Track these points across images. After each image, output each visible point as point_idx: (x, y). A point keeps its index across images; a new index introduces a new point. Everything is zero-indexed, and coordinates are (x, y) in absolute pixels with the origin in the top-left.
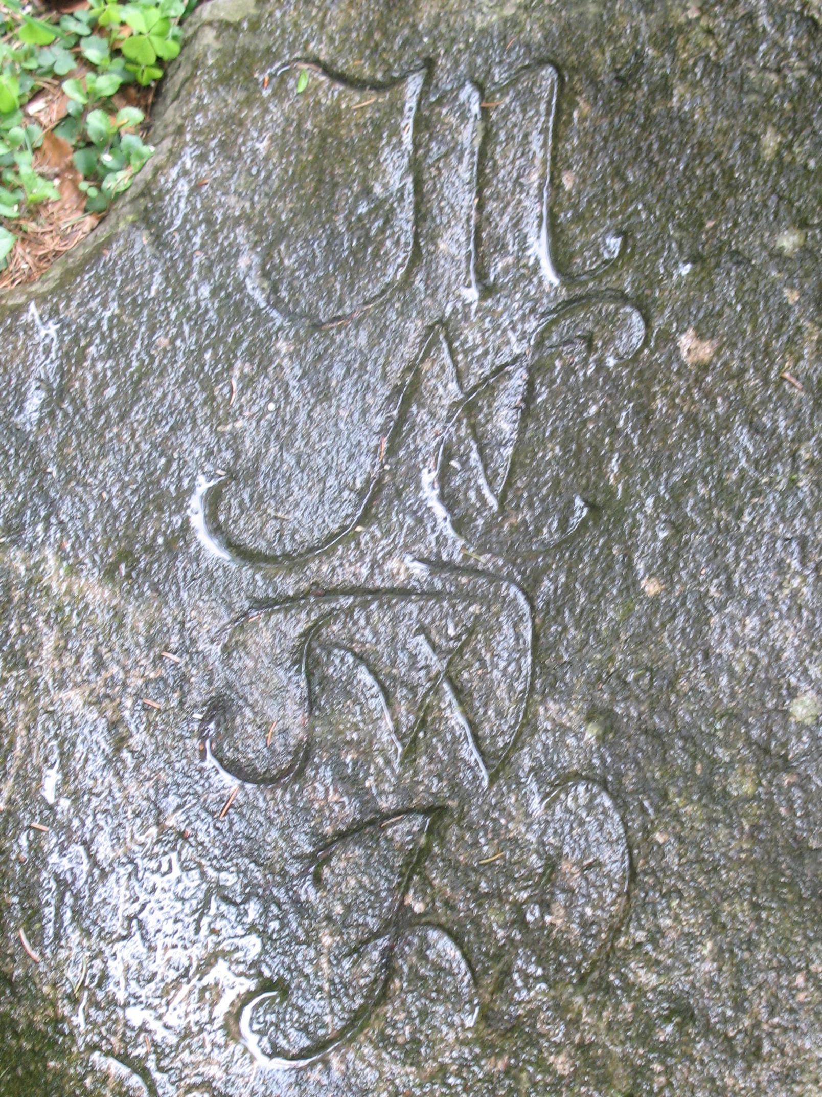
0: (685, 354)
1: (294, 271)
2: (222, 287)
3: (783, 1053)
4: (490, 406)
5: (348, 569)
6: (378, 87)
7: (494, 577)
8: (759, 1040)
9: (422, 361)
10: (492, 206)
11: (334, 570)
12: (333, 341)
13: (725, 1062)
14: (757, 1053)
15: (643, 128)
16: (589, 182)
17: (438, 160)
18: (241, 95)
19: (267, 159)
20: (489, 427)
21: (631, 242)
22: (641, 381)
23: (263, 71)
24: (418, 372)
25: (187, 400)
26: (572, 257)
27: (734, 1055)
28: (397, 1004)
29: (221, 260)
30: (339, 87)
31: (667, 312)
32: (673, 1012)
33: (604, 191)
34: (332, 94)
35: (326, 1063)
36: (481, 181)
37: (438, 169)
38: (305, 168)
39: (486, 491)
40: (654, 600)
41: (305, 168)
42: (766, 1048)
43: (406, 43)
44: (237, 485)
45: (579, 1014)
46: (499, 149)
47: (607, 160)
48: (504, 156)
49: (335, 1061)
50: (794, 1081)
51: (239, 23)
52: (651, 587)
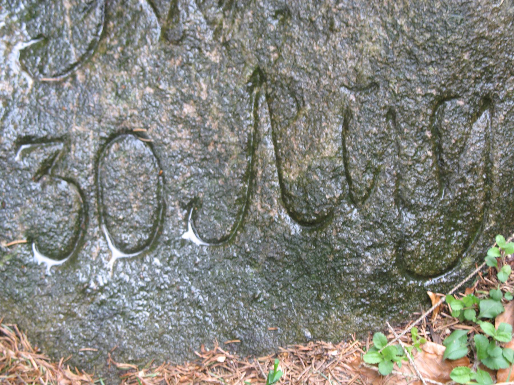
3: (347, 25)
8: (332, 19)
13: (313, 38)
14: (332, 29)
27: (317, 31)
28: (113, 35)
32: (278, 12)
35: (74, 76)
42: (337, 24)
45: (221, 24)
49: (80, 77)
50: (357, 41)
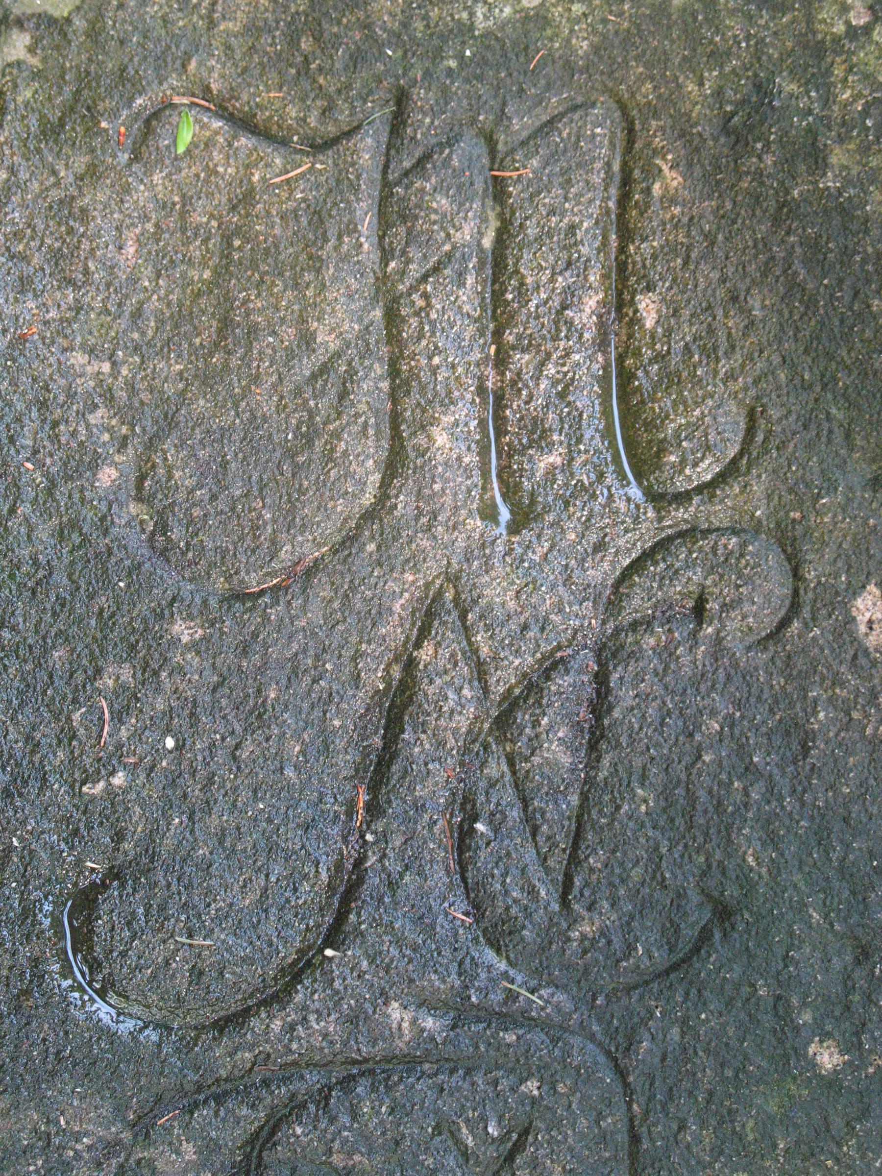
0: (863, 629)
1: (191, 491)
2: (74, 525)
4: (536, 724)
5: (312, 1026)
6: (319, 146)
7: (556, 1031)
9: (418, 645)
10: (521, 360)
11: (292, 1028)
12: (266, 618)
15: (776, 221)
16: (686, 313)
17: (425, 278)
18: (81, 162)
19: (133, 280)
20: (536, 760)
21: (762, 423)
22: (789, 678)
23: (114, 114)
24: (410, 665)
25: (28, 738)
26: (661, 452)
29: (68, 478)
30: (244, 142)
31: (829, 554)
33: (711, 330)
34: (236, 158)
36: (498, 313)
37: (426, 296)
38: (198, 295)
39: (535, 873)
40: (831, 1083)
41: (198, 295)
43: (356, 59)
44: (122, 886)
46: (527, 256)
47: (715, 275)
48: (534, 267)
51: (68, 20)
52: (828, 1058)
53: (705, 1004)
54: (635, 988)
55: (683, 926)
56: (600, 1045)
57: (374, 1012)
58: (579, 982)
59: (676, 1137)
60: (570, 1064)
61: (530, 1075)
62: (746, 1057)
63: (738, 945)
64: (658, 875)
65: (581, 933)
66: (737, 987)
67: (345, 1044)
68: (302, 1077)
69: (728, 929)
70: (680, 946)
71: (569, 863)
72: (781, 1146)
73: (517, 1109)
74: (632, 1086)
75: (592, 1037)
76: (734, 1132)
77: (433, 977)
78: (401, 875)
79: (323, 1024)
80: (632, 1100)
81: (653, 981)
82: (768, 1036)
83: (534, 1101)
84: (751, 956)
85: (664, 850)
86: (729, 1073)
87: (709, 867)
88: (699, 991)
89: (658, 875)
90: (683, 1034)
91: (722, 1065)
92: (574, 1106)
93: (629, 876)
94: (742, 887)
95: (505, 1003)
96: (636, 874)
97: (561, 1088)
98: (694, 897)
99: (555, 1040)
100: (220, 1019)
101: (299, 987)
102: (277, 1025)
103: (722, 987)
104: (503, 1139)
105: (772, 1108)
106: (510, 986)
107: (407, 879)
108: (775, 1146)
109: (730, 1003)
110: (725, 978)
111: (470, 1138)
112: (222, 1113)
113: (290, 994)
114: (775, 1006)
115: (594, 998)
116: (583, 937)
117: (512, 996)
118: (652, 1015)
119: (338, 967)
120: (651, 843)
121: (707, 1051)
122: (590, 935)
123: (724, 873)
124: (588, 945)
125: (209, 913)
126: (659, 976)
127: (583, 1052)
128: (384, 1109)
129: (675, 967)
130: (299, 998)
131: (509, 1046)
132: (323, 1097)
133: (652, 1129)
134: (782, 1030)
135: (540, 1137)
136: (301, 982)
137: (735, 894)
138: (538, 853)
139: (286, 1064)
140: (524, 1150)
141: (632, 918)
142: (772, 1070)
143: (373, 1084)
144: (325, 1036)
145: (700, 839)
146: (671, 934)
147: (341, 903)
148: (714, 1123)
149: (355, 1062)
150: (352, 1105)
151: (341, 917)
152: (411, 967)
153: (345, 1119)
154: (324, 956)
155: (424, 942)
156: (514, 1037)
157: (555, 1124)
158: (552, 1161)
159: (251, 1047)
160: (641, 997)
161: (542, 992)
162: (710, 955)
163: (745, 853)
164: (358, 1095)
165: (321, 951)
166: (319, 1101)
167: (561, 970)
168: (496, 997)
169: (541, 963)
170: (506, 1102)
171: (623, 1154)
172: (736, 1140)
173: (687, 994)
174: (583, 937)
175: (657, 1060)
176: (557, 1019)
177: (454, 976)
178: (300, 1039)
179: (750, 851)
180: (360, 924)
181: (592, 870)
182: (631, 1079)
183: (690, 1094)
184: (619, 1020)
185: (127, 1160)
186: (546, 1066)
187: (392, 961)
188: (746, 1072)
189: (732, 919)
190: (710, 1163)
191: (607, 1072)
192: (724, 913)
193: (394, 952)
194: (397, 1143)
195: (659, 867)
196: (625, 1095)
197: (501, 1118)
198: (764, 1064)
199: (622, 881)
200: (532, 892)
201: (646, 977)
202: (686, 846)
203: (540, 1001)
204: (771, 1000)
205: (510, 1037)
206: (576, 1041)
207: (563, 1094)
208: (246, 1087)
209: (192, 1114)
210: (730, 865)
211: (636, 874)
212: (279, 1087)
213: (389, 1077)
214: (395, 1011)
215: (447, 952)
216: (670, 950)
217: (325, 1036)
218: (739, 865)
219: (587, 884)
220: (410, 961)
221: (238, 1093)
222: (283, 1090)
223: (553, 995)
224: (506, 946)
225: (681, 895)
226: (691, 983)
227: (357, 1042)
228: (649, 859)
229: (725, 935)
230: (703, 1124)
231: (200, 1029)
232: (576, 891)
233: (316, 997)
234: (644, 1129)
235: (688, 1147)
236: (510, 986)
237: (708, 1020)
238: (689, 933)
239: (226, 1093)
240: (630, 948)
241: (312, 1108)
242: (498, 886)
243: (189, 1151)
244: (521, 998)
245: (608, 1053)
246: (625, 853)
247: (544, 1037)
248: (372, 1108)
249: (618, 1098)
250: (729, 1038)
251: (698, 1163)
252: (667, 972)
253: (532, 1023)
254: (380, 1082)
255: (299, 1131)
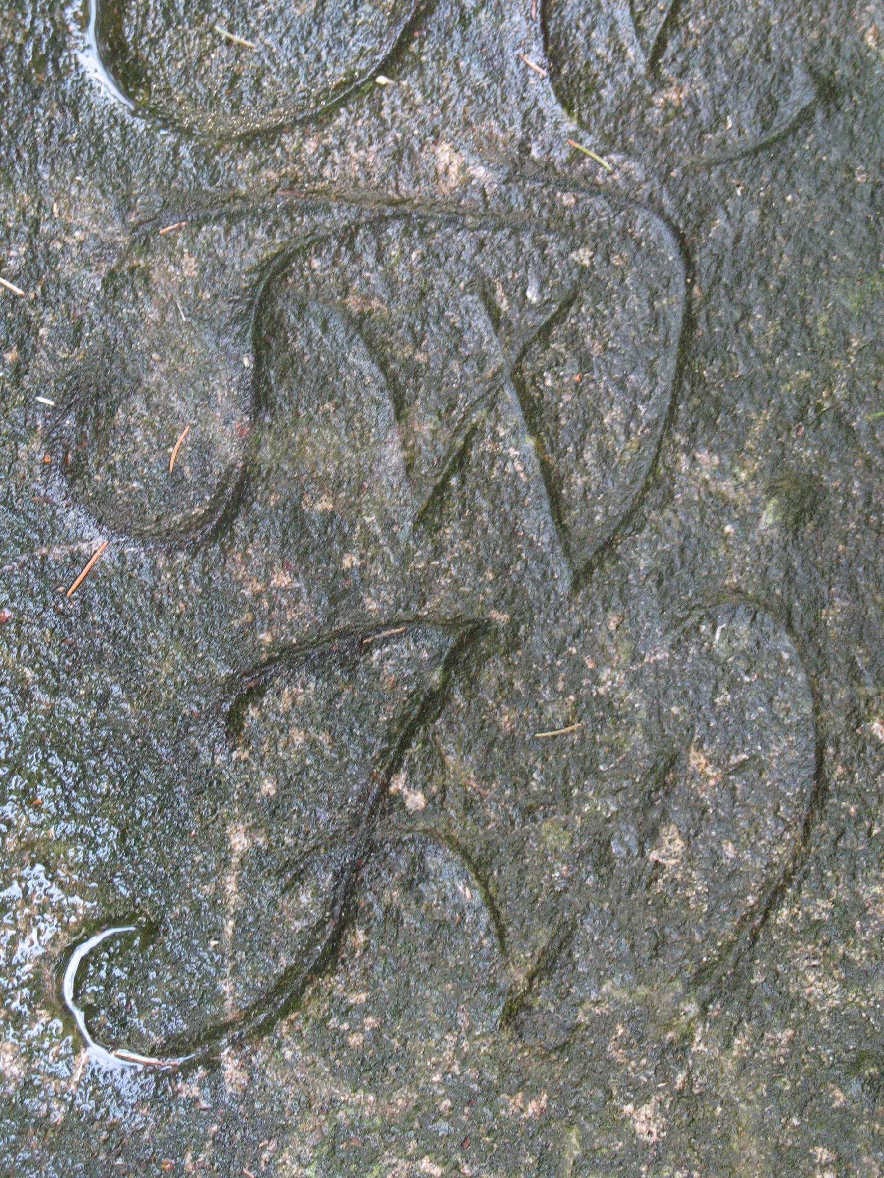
5: (352, 154)
7: (621, 200)
11: (327, 151)
39: (626, 31)
53: (793, 186)
54: (717, 164)
55: (782, 103)
56: (668, 220)
57: (421, 150)
58: (655, 152)
59: (736, 325)
60: (631, 234)
61: (584, 242)
62: (831, 245)
63: (840, 127)
64: (764, 47)
65: (666, 100)
66: (833, 170)
67: (383, 178)
68: (328, 210)
69: (833, 110)
70: (775, 124)
71: (665, 25)
72: (855, 344)
73: (563, 277)
74: (697, 267)
75: (660, 212)
76: (804, 325)
77: (493, 123)
78: (476, 12)
79: (362, 153)
80: (693, 282)
81: (739, 158)
82: (859, 226)
83: (583, 270)
84: (854, 140)
85: (774, 21)
86: (809, 261)
87: (822, 43)
88: (789, 172)
89: (764, 47)
90: (763, 215)
91: (802, 253)
92: (628, 281)
93: (730, 45)
94: (855, 67)
95: (569, 162)
96: (739, 43)
97: (615, 260)
98: (799, 74)
99: (617, 209)
100: (248, 133)
101: (342, 110)
102: (310, 146)
103: (817, 168)
104: (544, 305)
105: (851, 305)
106: (577, 146)
107: (482, 15)
108: (848, 344)
109: (821, 188)
110: (820, 160)
111: (505, 302)
112: (234, 232)
113: (331, 116)
114: (873, 194)
115: (670, 170)
116: (668, 105)
117: (577, 157)
118: (731, 194)
119: (389, 96)
120: (761, 13)
121: (787, 236)
122: (676, 104)
123: (838, 51)
124: (672, 112)
125: (256, 13)
126: (746, 154)
127: (649, 227)
128: (414, 256)
129: (765, 146)
130: (341, 121)
131: (565, 208)
132: (348, 236)
133: (712, 314)
134: (877, 221)
135: (583, 309)
136: (345, 106)
137: (847, 74)
138: (632, 12)
139: (314, 192)
140: (564, 321)
141: (726, 89)
142: (858, 263)
143: (406, 229)
144: (363, 165)
145: (817, 14)
146: (769, 107)
147: (403, 33)
148: (782, 313)
149: (392, 203)
150: (379, 245)
151: (401, 47)
152: (470, 109)
153: (369, 259)
154: (376, 84)
155: (489, 86)
156: (573, 200)
157: (602, 296)
158: (593, 337)
159: (277, 165)
160: (723, 174)
161: (612, 156)
162: (807, 135)
163: (865, 31)
164: (388, 236)
165: (373, 78)
166: (343, 238)
167: (637, 137)
168: (560, 156)
169: (616, 128)
170: (552, 268)
171: (674, 340)
172: (804, 335)
173: (774, 175)
174: (668, 105)
175: (728, 242)
176: (624, 187)
177: (517, 125)
178: (334, 163)
179: (871, 30)
180: (421, 54)
181: (688, 34)
182: (697, 258)
183: (762, 280)
184: (693, 196)
185: (119, 266)
186: (604, 235)
187: (450, 99)
188: (828, 262)
189: (839, 101)
190: (771, 358)
191: (671, 249)
192: (829, 92)
193: (455, 88)
194: (423, 295)
195: (765, 39)
196: (687, 277)
197: (543, 283)
198: (850, 255)
199: (721, 49)
200: (619, 52)
201: (731, 155)
202: (799, 20)
203: (609, 166)
204: (868, 188)
205: (568, 199)
206: (642, 215)
207: (616, 267)
208: (264, 210)
209: (200, 227)
210: (847, 48)
211: (739, 43)
212: (302, 216)
213: (425, 225)
214: (444, 154)
215: (513, 99)
216: (763, 127)
217: (363, 165)
218: (856, 44)
219: (681, 49)
220: (471, 102)
221: (254, 215)
222: (306, 219)
223: (623, 162)
224: (580, 104)
225: (785, 70)
226: (782, 162)
227: (396, 178)
228: (756, 30)
229: (828, 116)
230: (770, 314)
231: (225, 138)
232: (668, 54)
233: (359, 123)
234: (703, 314)
235: (750, 337)
236: (577, 146)
237: (794, 203)
238: (789, 111)
239: (240, 214)
240: (718, 120)
241: (334, 243)
242: (582, 40)
243: (190, 266)
244: (587, 160)
245: (675, 230)
246: (729, 21)
247: (605, 204)
248: (402, 252)
249: (679, 280)
250: (815, 223)
251: (757, 355)
252: (756, 152)
253: (595, 190)
254: (414, 228)
255: (316, 263)
